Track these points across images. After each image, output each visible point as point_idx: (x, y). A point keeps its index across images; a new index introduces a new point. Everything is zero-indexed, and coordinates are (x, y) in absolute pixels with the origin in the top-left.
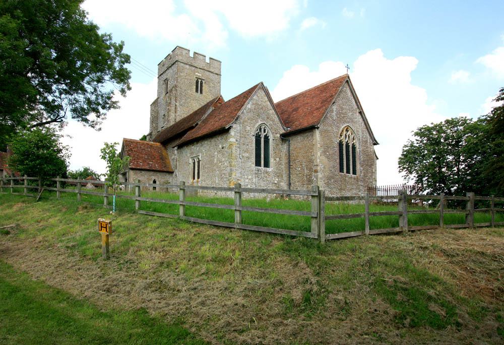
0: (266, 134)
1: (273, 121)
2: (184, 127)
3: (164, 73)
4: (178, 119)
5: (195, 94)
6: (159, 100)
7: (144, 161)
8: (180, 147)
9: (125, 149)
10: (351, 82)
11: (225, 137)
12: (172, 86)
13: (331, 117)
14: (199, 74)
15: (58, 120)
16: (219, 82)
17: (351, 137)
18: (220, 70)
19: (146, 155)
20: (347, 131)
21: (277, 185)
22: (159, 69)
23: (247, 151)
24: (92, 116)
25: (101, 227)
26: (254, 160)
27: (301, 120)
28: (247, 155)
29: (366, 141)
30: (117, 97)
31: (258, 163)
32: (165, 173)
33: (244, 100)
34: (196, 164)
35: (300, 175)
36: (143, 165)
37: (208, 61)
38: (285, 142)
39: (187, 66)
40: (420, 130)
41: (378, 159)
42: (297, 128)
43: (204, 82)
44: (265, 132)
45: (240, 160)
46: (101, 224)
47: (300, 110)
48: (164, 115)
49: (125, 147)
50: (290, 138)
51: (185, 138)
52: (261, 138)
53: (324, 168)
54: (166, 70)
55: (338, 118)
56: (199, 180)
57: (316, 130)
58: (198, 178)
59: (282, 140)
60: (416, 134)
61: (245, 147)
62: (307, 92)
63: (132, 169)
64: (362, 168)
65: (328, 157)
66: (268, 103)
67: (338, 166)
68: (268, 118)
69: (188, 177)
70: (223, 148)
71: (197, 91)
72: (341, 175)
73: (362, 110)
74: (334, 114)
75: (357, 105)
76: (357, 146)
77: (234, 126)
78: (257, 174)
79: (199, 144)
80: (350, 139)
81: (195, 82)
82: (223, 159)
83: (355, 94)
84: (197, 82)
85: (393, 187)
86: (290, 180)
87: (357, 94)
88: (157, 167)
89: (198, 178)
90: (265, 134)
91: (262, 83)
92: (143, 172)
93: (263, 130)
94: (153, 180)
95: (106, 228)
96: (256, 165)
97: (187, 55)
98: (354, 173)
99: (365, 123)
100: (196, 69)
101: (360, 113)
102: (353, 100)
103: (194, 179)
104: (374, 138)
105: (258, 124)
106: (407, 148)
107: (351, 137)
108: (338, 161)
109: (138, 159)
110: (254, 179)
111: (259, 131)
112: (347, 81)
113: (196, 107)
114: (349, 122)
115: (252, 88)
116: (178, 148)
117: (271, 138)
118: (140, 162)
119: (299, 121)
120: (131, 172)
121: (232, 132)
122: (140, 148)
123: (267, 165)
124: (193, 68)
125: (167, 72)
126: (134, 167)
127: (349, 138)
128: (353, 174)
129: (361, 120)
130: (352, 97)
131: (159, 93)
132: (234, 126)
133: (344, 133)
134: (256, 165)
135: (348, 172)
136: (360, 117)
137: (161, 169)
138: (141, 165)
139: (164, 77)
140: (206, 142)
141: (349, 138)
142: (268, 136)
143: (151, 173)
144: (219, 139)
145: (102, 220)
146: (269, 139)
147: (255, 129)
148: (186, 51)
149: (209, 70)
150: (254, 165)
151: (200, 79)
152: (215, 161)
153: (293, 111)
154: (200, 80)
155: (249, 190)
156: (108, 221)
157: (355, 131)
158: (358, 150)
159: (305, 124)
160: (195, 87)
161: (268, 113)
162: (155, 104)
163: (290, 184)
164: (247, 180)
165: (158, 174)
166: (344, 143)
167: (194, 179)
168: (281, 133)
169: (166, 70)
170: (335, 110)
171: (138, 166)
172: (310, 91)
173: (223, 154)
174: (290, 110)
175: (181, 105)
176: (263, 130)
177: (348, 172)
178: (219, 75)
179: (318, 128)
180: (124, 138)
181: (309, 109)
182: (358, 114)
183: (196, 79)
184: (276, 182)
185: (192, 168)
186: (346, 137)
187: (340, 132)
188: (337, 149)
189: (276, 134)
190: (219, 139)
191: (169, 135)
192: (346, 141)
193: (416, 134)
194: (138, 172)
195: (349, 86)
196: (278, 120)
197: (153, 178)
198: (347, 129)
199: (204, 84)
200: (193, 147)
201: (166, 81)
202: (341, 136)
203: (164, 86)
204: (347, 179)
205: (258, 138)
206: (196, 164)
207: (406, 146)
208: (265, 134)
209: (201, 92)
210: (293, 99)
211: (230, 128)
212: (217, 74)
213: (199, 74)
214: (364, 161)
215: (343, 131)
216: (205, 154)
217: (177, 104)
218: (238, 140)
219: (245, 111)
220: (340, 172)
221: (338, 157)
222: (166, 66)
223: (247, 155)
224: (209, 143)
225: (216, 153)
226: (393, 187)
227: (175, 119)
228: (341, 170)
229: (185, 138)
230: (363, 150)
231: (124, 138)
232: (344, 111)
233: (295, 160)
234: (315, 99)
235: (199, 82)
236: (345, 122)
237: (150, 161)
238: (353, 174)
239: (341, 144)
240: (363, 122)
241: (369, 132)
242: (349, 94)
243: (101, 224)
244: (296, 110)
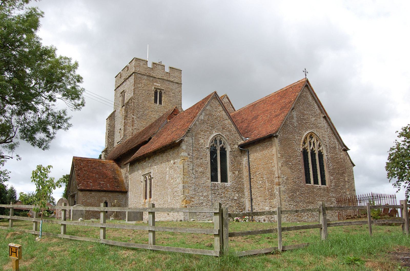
0: (223, 146)
1: (230, 131)
2: (138, 142)
3: (120, 85)
4: (135, 132)
5: (153, 105)
6: (116, 113)
7: (95, 181)
8: (132, 163)
9: (75, 169)
10: (310, 86)
11: (176, 150)
12: (129, 98)
13: (292, 124)
14: (157, 84)
15: (8, 141)
16: (180, 91)
17: (317, 144)
18: (180, 78)
19: (97, 174)
20: (311, 137)
21: (238, 202)
22: (116, 82)
23: (201, 165)
24: (40, 136)
25: (12, 252)
26: (209, 175)
27: (260, 129)
28: (201, 169)
29: (335, 148)
30: (71, 113)
31: (214, 178)
32: (117, 194)
33: (197, 111)
34: (148, 181)
35: (262, 189)
36: (93, 186)
37: (167, 70)
38: (244, 153)
39: (145, 77)
40: (405, 130)
41: (354, 165)
42: (256, 138)
43: (163, 91)
44: (221, 144)
45: (193, 176)
46: (12, 248)
47: (260, 118)
48: (120, 129)
49: (75, 166)
50: (249, 149)
51: (137, 154)
52: (216, 150)
53: (287, 179)
54: (123, 82)
55: (299, 124)
56: (152, 199)
57: (275, 138)
58: (150, 197)
59: (241, 151)
60: (401, 135)
61: (199, 161)
62: (267, 99)
63: (81, 190)
64: (332, 178)
65: (291, 168)
66: (223, 113)
67: (303, 177)
68: (223, 129)
69: (140, 197)
70: (174, 163)
71: (156, 101)
72: (307, 186)
73: (326, 114)
74: (295, 120)
75: (320, 110)
76: (325, 153)
77: (186, 139)
78: (214, 190)
79: (151, 160)
80: (316, 146)
81: (153, 92)
82: (175, 175)
83: (316, 99)
84: (156, 93)
85: (362, 196)
86: (251, 195)
87: (319, 98)
88: (109, 187)
89: (150, 197)
90: (221, 145)
91: (215, 93)
92: (93, 193)
93: (218, 141)
94: (104, 201)
95: (16, 252)
96: (212, 180)
97: (145, 66)
98: (323, 183)
99: (331, 128)
100: (154, 80)
101: (325, 117)
102: (315, 104)
103: (146, 199)
104: (343, 144)
105: (212, 136)
106: (394, 151)
107: (317, 144)
108: (303, 171)
109: (89, 179)
110: (210, 196)
111: (214, 143)
112: (307, 86)
113: (155, 116)
114: (312, 128)
115: (206, 98)
116: (130, 165)
117: (228, 150)
118: (91, 183)
119: (258, 129)
120: (80, 194)
121: (184, 146)
122: (91, 166)
123: (224, 179)
124: (152, 79)
125: (124, 84)
126: (83, 188)
127: (314, 145)
128: (322, 184)
129: (326, 125)
130: (314, 102)
131: (116, 105)
132: (186, 139)
133: (308, 140)
134: (212, 180)
135: (316, 182)
136: (325, 121)
137: (113, 189)
138: (92, 185)
139: (121, 89)
140: (158, 158)
141: (314, 145)
142: (225, 148)
143: (102, 194)
144: (171, 154)
145: (12, 245)
146: (226, 151)
147: (209, 142)
148: (144, 63)
149: (169, 79)
150: (210, 180)
151: (159, 89)
152: (167, 178)
153: (253, 119)
154: (159, 91)
155: (162, 210)
156: (18, 246)
157: (321, 137)
158: (325, 158)
159: (264, 133)
160: (153, 98)
161: (224, 124)
162: (112, 117)
163: (252, 200)
164: (202, 198)
165: (110, 195)
166: (309, 151)
167: (146, 199)
168: (239, 143)
169: (123, 82)
170: (295, 116)
171: (87, 187)
172: (270, 97)
173: (175, 170)
174: (250, 118)
175: (139, 118)
176: (218, 141)
177: (316, 182)
178: (179, 84)
179: (276, 136)
180: (74, 157)
181: (269, 116)
182: (322, 119)
183: (155, 90)
184: (236, 198)
185: (144, 186)
186: (310, 144)
187: (303, 139)
188: (301, 158)
189: (234, 145)
190: (171, 154)
191: (124, 151)
192: (311, 148)
193: (401, 135)
194: (88, 193)
195: (309, 90)
196: (235, 130)
197: (105, 199)
198: (311, 135)
199: (163, 95)
200: (145, 163)
201: (123, 93)
202: (304, 143)
203: (121, 99)
204: (315, 190)
205: (213, 153)
206: (148, 181)
207: (392, 149)
208: (221, 145)
209: (160, 103)
210: (254, 106)
211: (181, 141)
212: (178, 83)
213: (157, 84)
214: (333, 169)
215: (306, 138)
216: (156, 171)
217: (135, 117)
218: (191, 154)
219: (197, 123)
220: (307, 183)
221: (303, 167)
222: (123, 78)
223: (201, 169)
224: (161, 158)
225: (168, 169)
226: (362, 196)
227: (132, 133)
228: (308, 181)
229: (137, 154)
230: (331, 157)
231: (74, 157)
232: (306, 116)
233: (255, 172)
234: (274, 105)
235: (158, 93)
236: (307, 129)
237: (101, 181)
238: (322, 184)
239: (305, 152)
240: (329, 127)
241: (336, 137)
242: (311, 99)
243: (12, 248)
244: (256, 118)
